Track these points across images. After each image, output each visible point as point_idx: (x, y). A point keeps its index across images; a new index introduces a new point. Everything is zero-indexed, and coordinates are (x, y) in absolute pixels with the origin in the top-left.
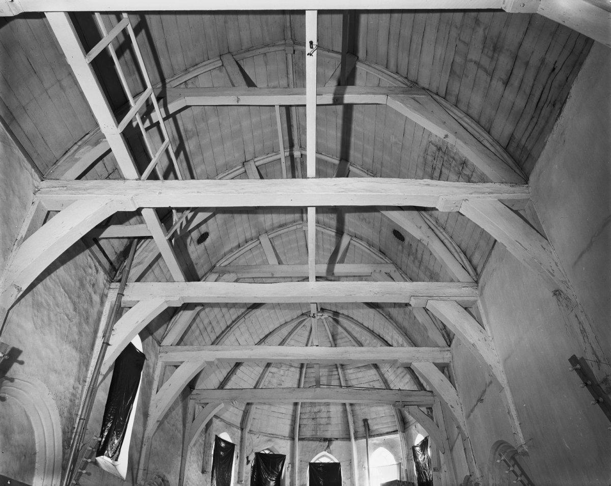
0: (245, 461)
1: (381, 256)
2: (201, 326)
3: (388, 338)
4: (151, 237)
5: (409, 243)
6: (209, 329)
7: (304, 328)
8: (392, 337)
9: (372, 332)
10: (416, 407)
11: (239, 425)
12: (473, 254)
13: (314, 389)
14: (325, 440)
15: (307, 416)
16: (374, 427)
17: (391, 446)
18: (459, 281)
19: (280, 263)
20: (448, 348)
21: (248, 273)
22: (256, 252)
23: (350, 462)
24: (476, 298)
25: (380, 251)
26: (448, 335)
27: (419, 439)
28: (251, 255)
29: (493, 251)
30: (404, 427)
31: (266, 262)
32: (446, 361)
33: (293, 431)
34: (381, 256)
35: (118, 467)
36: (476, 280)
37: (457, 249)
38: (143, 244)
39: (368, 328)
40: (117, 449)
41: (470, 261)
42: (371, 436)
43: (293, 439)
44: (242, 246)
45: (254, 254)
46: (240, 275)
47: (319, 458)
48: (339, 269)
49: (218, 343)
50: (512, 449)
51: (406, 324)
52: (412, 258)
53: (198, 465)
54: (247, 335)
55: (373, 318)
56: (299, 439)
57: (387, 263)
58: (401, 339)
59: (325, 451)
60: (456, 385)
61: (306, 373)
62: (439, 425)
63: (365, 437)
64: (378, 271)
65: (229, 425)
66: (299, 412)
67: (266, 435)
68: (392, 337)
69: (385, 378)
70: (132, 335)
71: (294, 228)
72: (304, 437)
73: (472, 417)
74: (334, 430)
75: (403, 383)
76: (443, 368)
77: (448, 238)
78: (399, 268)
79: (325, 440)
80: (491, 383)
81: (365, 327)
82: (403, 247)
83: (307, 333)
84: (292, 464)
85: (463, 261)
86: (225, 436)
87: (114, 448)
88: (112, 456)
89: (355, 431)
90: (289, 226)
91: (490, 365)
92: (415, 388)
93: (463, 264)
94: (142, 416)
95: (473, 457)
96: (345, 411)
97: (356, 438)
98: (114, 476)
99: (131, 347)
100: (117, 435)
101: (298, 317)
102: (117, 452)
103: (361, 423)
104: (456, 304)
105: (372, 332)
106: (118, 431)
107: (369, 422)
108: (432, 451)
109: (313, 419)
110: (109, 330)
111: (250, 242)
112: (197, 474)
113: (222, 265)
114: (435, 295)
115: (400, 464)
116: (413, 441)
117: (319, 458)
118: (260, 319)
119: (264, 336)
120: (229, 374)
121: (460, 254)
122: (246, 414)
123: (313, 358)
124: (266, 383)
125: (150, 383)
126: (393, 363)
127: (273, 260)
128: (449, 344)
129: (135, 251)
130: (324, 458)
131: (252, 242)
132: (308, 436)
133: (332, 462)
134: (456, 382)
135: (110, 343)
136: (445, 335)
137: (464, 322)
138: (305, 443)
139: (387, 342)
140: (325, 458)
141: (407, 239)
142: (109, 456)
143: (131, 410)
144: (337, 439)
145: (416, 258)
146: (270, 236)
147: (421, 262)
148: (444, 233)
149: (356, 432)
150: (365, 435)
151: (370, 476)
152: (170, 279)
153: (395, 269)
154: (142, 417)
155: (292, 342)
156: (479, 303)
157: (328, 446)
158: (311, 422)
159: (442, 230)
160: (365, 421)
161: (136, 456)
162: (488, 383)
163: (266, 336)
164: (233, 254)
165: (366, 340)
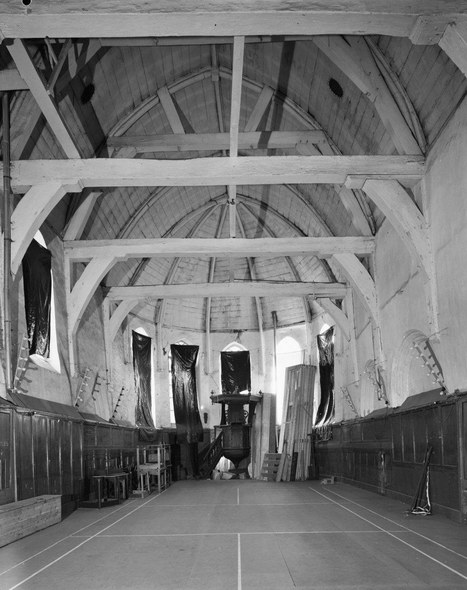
0: (162, 352)
1: (309, 120)
2: (102, 217)
3: (303, 227)
4: (29, 90)
5: (348, 98)
6: (111, 220)
7: (212, 217)
8: (309, 226)
9: (287, 220)
10: (328, 299)
11: (152, 320)
12: (429, 115)
13: (228, 284)
14: (235, 331)
15: (217, 310)
16: (281, 318)
17: (297, 336)
18: (405, 154)
19: (189, 129)
20: (373, 238)
21: (149, 145)
22: (155, 116)
23: (259, 351)
24: (419, 176)
25: (309, 112)
26: (375, 223)
27: (325, 328)
28: (149, 121)
29: (458, 110)
30: (311, 317)
31: (169, 130)
32: (368, 252)
33: (204, 324)
34: (309, 120)
35: (51, 363)
36: (424, 152)
37: (409, 107)
38: (15, 103)
39: (283, 216)
40: (46, 347)
41: (422, 125)
42: (278, 327)
43: (205, 331)
44: (138, 106)
45: (153, 118)
46: (140, 150)
47: (229, 348)
48: (276, 139)
49: (122, 236)
50: (423, 337)
51: (327, 210)
52: (348, 122)
53: (120, 357)
54: (152, 226)
55: (290, 204)
56: (211, 332)
57: (316, 130)
58: (319, 227)
59: (235, 341)
60: (375, 277)
61: (215, 268)
62: (348, 316)
63: (273, 328)
64: (304, 141)
65: (144, 321)
66: (209, 306)
67: (179, 328)
68: (309, 226)
69: (296, 271)
70: (32, 232)
71: (201, 77)
72: (215, 329)
73: (386, 307)
74: (245, 322)
75: (317, 275)
76: (364, 260)
77: (402, 90)
78: (329, 137)
79: (235, 331)
80: (416, 273)
81: (280, 214)
82: (339, 106)
83: (215, 224)
84: (205, 353)
85: (413, 125)
86: (141, 331)
87: (44, 347)
88: (44, 354)
89: (264, 323)
90: (195, 74)
91: (421, 256)
92: (327, 280)
93: (413, 130)
94: (61, 316)
95: (380, 344)
96: (255, 304)
97: (264, 329)
98: (50, 371)
99: (34, 243)
100: (43, 334)
101: (206, 204)
102: (47, 350)
103: (270, 315)
104: (397, 184)
105: (287, 220)
106: (44, 331)
107: (277, 314)
108: (336, 338)
109: (223, 312)
110: (6, 224)
111: (147, 101)
112: (121, 365)
113: (116, 135)
114: (375, 173)
115: (304, 351)
116: (318, 330)
117: (229, 348)
118: (165, 207)
119: (170, 227)
120: (138, 270)
121: (412, 115)
122: (158, 309)
123: (229, 251)
124: (176, 279)
125: (61, 282)
126: (304, 254)
127: (178, 128)
128: (374, 233)
129: (9, 113)
130: (235, 347)
131: (149, 101)
132: (219, 329)
133: (241, 350)
134: (375, 273)
135: (12, 238)
136: (372, 222)
137: (402, 207)
138: (216, 334)
139: (302, 231)
140: (235, 347)
141: (347, 93)
142: (40, 354)
143: (50, 310)
144: (246, 330)
145: (353, 122)
146: (172, 91)
147: (358, 128)
148: (397, 83)
149: (264, 324)
150: (273, 326)
151: (277, 363)
152: (61, 155)
153: (324, 138)
154: (62, 316)
155: (201, 234)
156: (423, 183)
157: (238, 337)
158: (221, 316)
159: (395, 79)
160: (274, 313)
161: (64, 352)
162: (412, 274)
163: (173, 227)
164: (127, 118)
165: (280, 229)
